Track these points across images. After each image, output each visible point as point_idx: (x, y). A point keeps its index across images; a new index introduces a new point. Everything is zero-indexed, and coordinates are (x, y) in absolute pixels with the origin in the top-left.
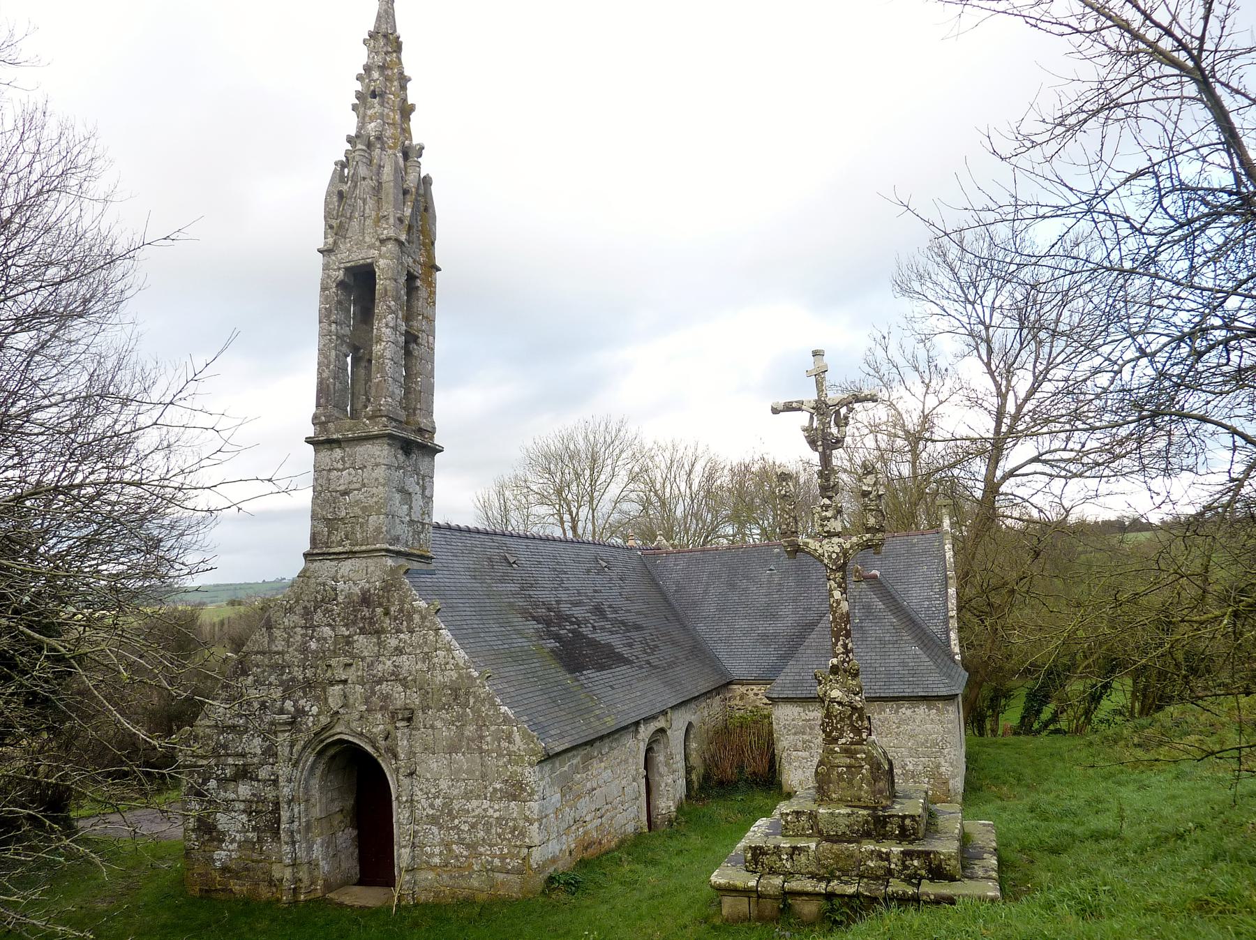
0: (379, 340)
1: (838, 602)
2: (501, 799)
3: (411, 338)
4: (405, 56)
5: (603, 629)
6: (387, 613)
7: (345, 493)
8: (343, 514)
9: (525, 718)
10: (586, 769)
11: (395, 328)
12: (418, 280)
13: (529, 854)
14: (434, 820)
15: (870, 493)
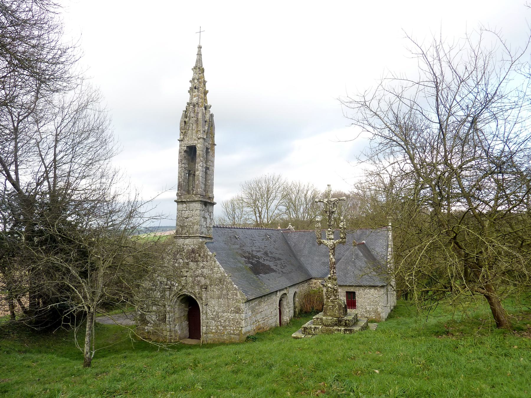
0: (198, 170)
3: (207, 168)
4: (205, 74)
5: (267, 260)
6: (199, 256)
7: (187, 218)
10: (260, 305)
11: (202, 167)
12: (209, 150)
14: (213, 319)
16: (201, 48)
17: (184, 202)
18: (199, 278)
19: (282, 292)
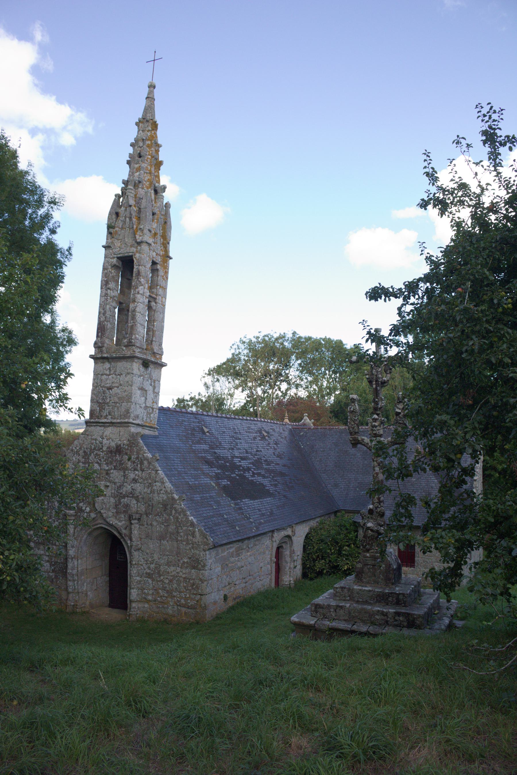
1: (377, 474)
2: (187, 567)
3: (152, 299)
5: (259, 474)
7: (110, 388)
8: (108, 400)
9: (203, 524)
10: (238, 555)
13: (201, 599)
14: (149, 575)
15: (400, 413)
16: (154, 87)
17: (107, 358)
18: (125, 500)
19: (283, 533)
